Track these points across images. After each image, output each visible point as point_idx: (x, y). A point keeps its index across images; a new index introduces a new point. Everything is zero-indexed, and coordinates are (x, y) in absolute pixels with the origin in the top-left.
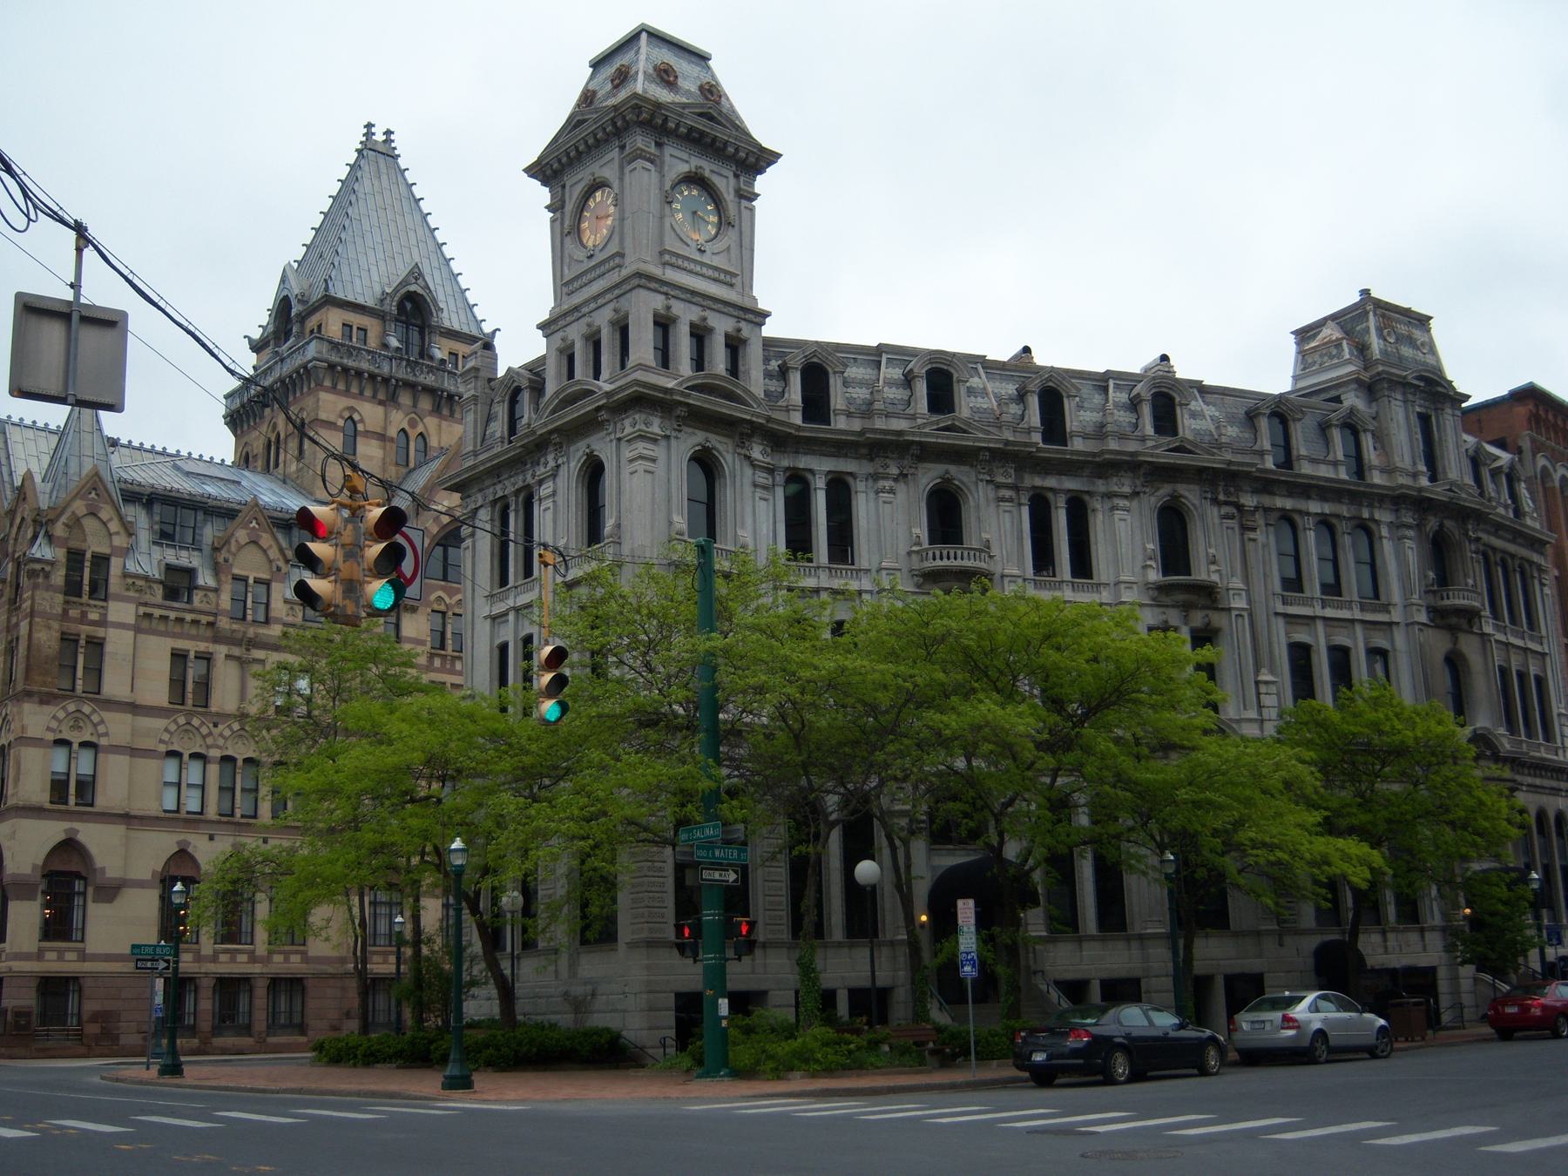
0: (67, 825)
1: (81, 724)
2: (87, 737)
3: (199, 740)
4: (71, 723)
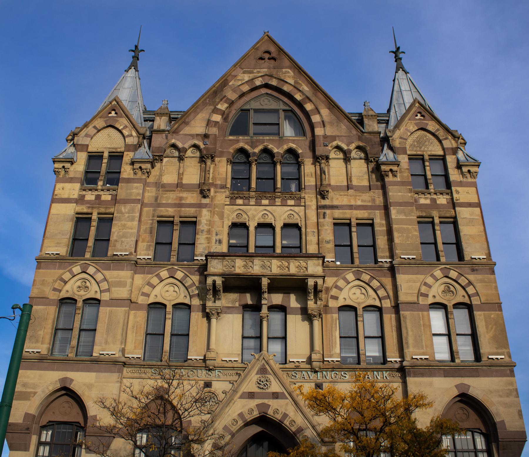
0: (458, 381)
1: (88, 284)
2: (460, 299)
3: (95, 287)
4: (79, 283)
